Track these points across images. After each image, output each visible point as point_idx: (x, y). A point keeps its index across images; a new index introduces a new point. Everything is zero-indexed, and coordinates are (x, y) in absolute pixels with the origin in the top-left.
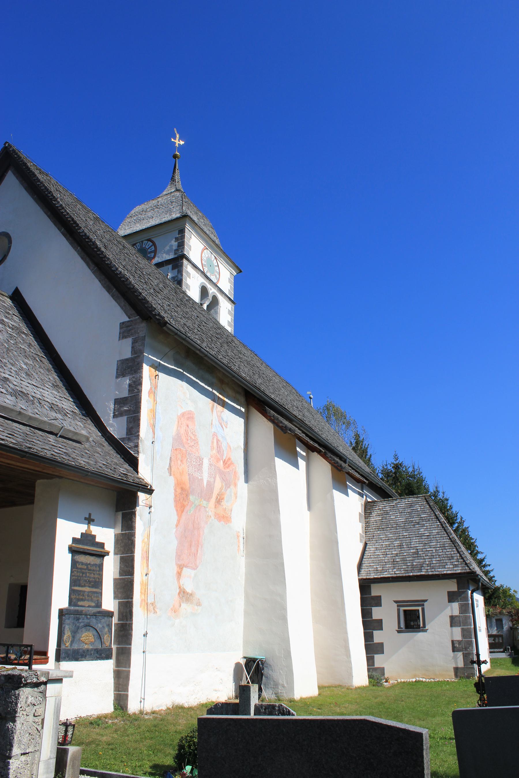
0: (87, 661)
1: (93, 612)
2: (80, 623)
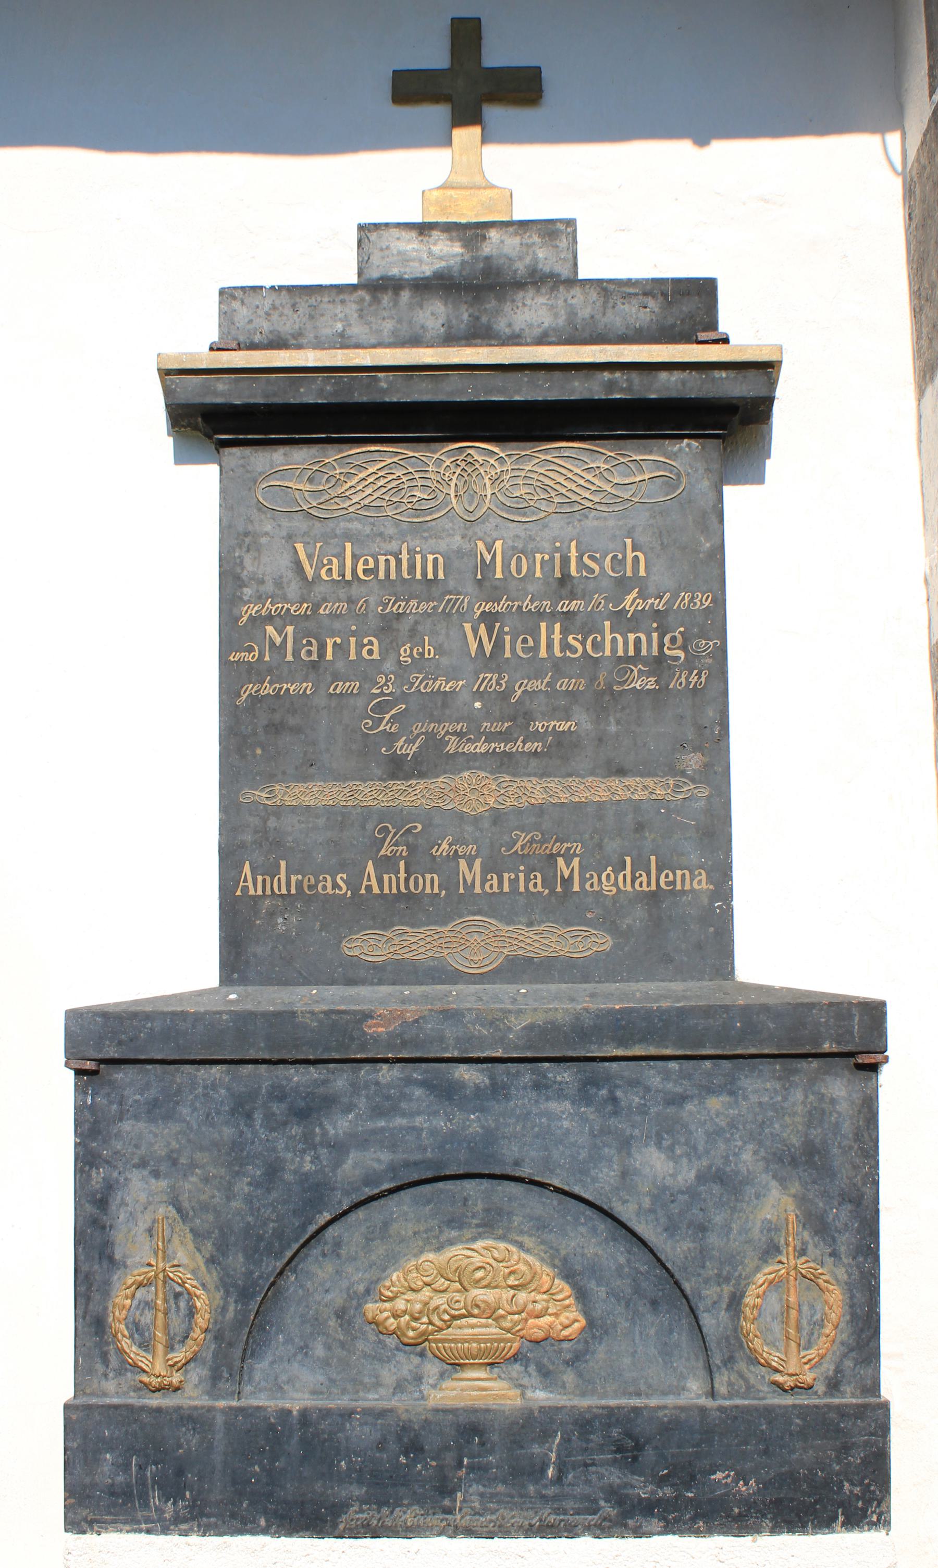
0: (470, 1532)
1: (518, 1024)
2: (339, 1148)
